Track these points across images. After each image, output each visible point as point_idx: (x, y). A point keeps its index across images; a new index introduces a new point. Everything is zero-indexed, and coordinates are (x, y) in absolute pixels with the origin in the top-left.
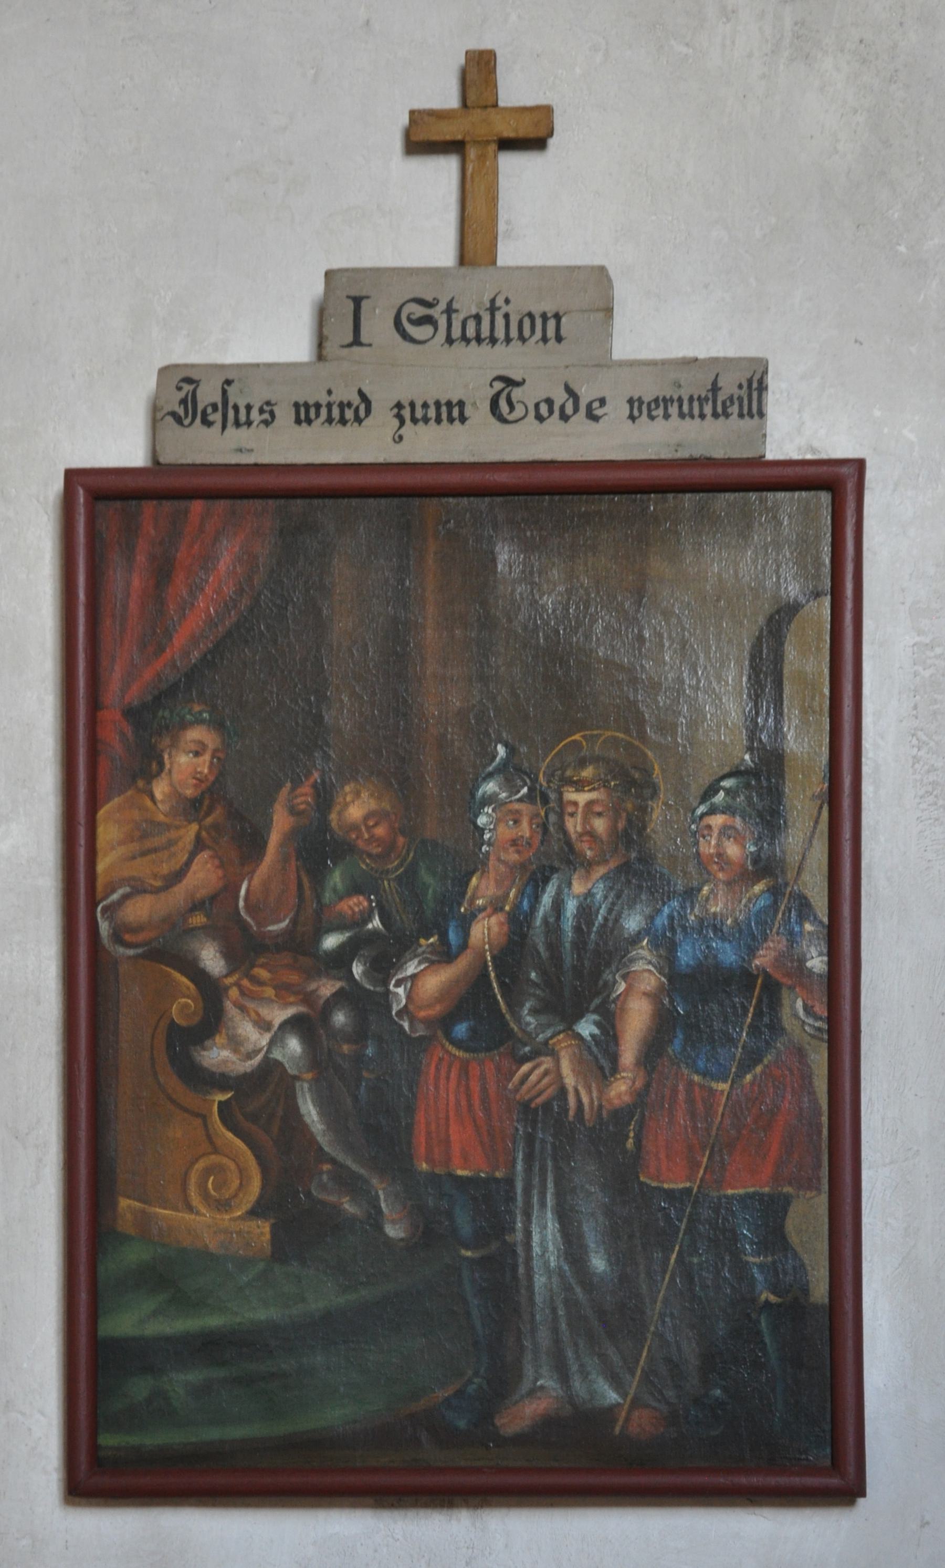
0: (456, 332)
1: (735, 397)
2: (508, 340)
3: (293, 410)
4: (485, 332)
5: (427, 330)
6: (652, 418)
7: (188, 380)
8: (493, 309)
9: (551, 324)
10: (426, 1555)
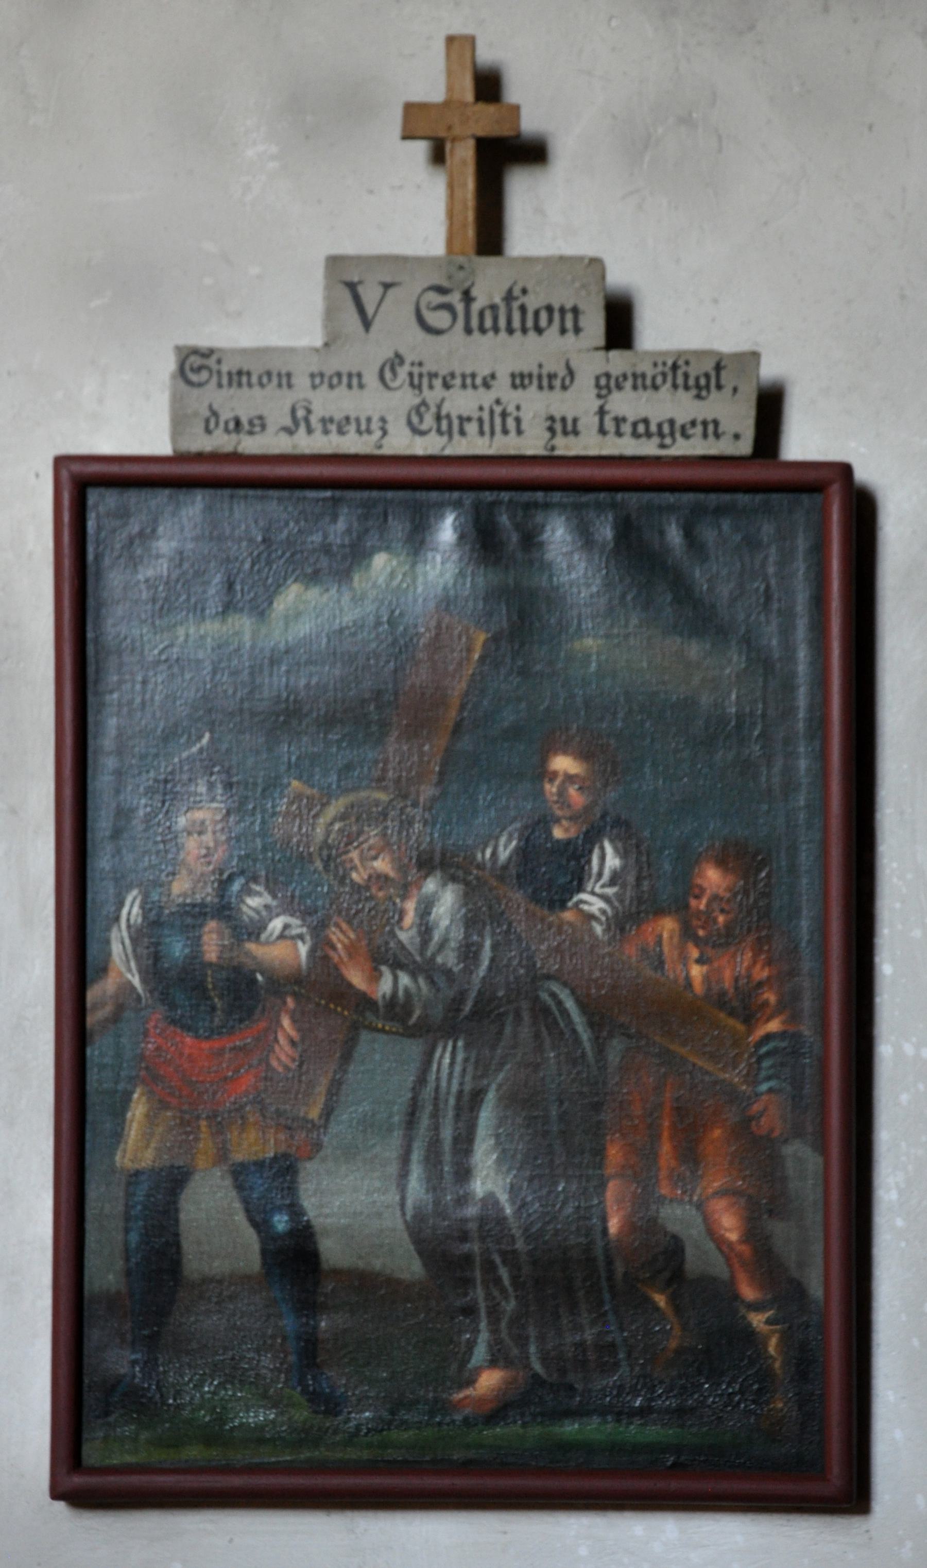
0: (475, 322)
2: (524, 330)
9: (569, 317)
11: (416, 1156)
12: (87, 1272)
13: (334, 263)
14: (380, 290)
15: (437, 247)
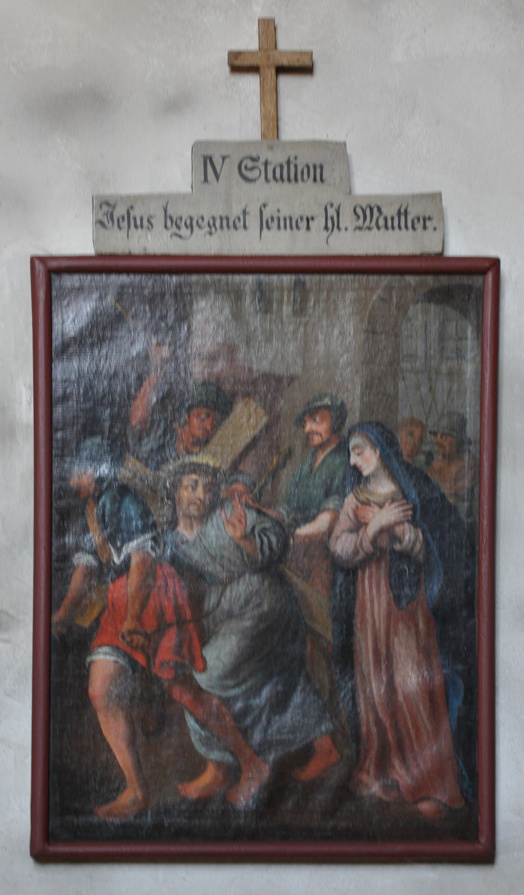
0: (270, 175)
7: (108, 204)
9: (318, 171)
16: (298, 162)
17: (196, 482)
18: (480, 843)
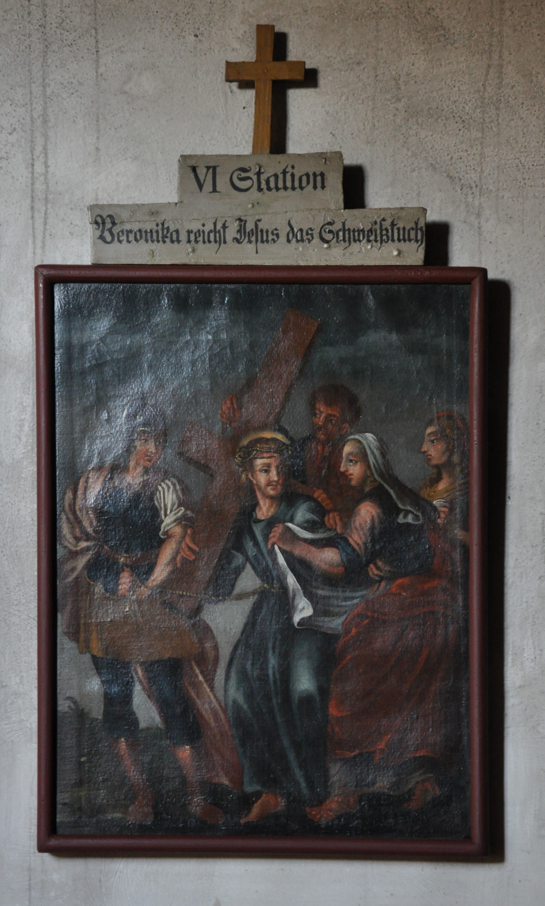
0: (264, 186)
1: (201, 230)
3: (226, 240)
4: (281, 185)
5: (248, 183)
6: (120, 242)
8: (284, 172)
9: (319, 178)
10: (17, 127)
11: (233, 675)
12: (59, 683)
13: (184, 158)
14: (206, 169)
15: (247, 150)
16: (295, 171)
17: (269, 466)
18: (142, 664)
